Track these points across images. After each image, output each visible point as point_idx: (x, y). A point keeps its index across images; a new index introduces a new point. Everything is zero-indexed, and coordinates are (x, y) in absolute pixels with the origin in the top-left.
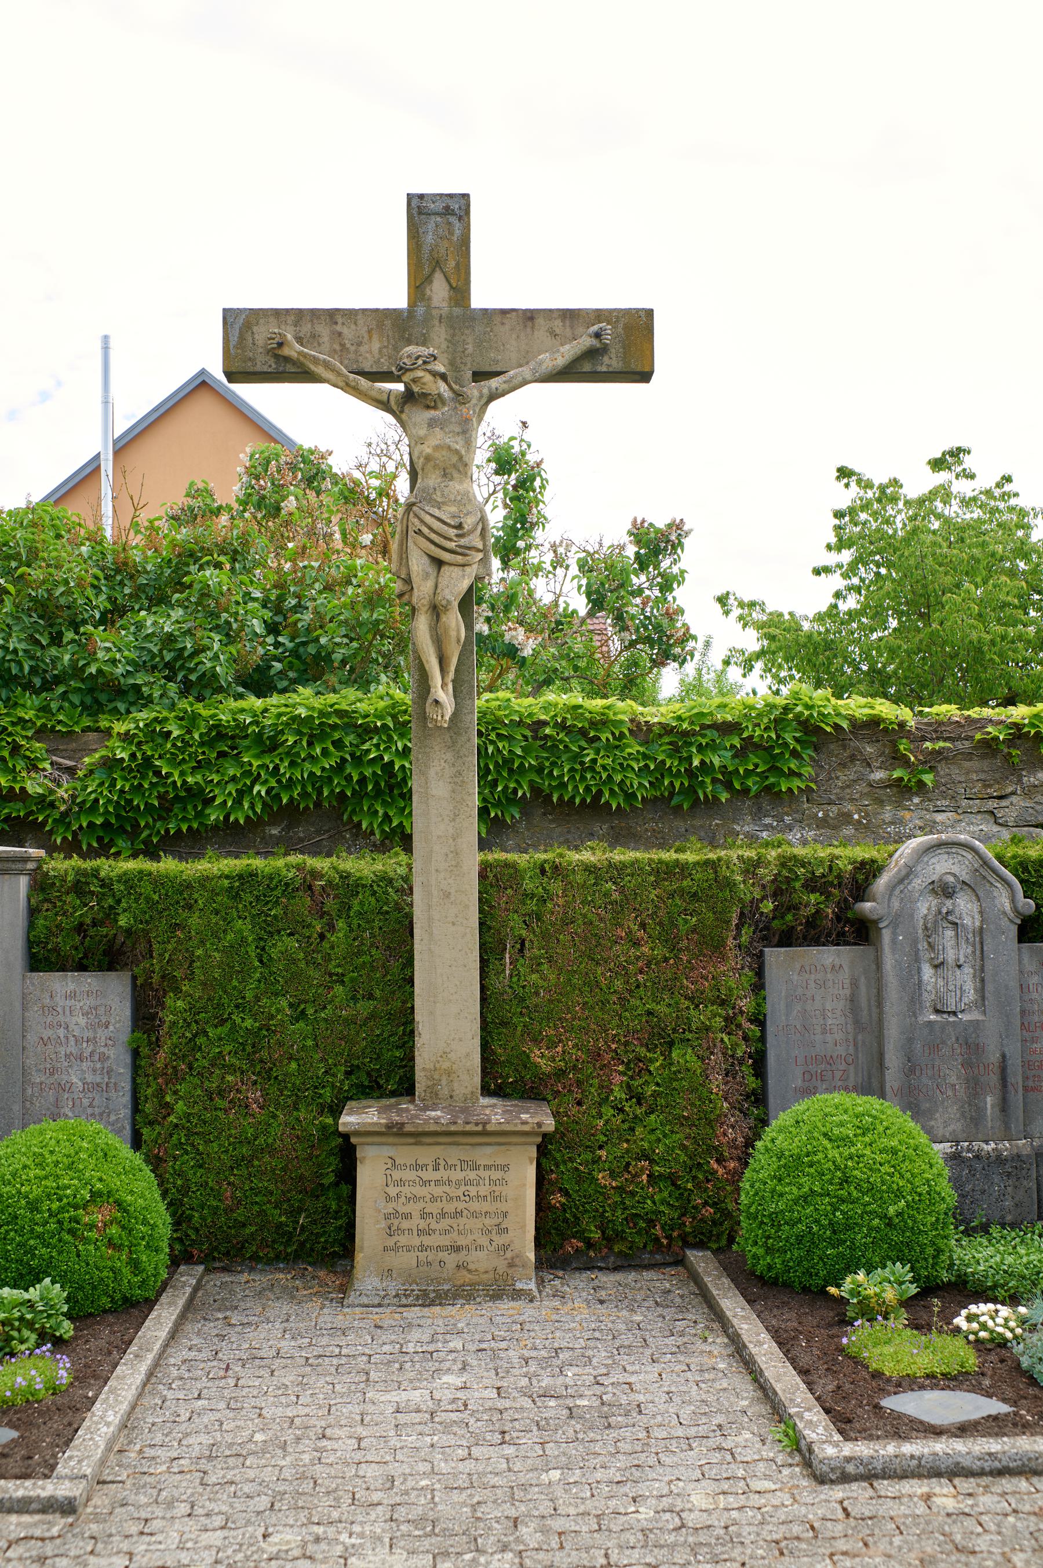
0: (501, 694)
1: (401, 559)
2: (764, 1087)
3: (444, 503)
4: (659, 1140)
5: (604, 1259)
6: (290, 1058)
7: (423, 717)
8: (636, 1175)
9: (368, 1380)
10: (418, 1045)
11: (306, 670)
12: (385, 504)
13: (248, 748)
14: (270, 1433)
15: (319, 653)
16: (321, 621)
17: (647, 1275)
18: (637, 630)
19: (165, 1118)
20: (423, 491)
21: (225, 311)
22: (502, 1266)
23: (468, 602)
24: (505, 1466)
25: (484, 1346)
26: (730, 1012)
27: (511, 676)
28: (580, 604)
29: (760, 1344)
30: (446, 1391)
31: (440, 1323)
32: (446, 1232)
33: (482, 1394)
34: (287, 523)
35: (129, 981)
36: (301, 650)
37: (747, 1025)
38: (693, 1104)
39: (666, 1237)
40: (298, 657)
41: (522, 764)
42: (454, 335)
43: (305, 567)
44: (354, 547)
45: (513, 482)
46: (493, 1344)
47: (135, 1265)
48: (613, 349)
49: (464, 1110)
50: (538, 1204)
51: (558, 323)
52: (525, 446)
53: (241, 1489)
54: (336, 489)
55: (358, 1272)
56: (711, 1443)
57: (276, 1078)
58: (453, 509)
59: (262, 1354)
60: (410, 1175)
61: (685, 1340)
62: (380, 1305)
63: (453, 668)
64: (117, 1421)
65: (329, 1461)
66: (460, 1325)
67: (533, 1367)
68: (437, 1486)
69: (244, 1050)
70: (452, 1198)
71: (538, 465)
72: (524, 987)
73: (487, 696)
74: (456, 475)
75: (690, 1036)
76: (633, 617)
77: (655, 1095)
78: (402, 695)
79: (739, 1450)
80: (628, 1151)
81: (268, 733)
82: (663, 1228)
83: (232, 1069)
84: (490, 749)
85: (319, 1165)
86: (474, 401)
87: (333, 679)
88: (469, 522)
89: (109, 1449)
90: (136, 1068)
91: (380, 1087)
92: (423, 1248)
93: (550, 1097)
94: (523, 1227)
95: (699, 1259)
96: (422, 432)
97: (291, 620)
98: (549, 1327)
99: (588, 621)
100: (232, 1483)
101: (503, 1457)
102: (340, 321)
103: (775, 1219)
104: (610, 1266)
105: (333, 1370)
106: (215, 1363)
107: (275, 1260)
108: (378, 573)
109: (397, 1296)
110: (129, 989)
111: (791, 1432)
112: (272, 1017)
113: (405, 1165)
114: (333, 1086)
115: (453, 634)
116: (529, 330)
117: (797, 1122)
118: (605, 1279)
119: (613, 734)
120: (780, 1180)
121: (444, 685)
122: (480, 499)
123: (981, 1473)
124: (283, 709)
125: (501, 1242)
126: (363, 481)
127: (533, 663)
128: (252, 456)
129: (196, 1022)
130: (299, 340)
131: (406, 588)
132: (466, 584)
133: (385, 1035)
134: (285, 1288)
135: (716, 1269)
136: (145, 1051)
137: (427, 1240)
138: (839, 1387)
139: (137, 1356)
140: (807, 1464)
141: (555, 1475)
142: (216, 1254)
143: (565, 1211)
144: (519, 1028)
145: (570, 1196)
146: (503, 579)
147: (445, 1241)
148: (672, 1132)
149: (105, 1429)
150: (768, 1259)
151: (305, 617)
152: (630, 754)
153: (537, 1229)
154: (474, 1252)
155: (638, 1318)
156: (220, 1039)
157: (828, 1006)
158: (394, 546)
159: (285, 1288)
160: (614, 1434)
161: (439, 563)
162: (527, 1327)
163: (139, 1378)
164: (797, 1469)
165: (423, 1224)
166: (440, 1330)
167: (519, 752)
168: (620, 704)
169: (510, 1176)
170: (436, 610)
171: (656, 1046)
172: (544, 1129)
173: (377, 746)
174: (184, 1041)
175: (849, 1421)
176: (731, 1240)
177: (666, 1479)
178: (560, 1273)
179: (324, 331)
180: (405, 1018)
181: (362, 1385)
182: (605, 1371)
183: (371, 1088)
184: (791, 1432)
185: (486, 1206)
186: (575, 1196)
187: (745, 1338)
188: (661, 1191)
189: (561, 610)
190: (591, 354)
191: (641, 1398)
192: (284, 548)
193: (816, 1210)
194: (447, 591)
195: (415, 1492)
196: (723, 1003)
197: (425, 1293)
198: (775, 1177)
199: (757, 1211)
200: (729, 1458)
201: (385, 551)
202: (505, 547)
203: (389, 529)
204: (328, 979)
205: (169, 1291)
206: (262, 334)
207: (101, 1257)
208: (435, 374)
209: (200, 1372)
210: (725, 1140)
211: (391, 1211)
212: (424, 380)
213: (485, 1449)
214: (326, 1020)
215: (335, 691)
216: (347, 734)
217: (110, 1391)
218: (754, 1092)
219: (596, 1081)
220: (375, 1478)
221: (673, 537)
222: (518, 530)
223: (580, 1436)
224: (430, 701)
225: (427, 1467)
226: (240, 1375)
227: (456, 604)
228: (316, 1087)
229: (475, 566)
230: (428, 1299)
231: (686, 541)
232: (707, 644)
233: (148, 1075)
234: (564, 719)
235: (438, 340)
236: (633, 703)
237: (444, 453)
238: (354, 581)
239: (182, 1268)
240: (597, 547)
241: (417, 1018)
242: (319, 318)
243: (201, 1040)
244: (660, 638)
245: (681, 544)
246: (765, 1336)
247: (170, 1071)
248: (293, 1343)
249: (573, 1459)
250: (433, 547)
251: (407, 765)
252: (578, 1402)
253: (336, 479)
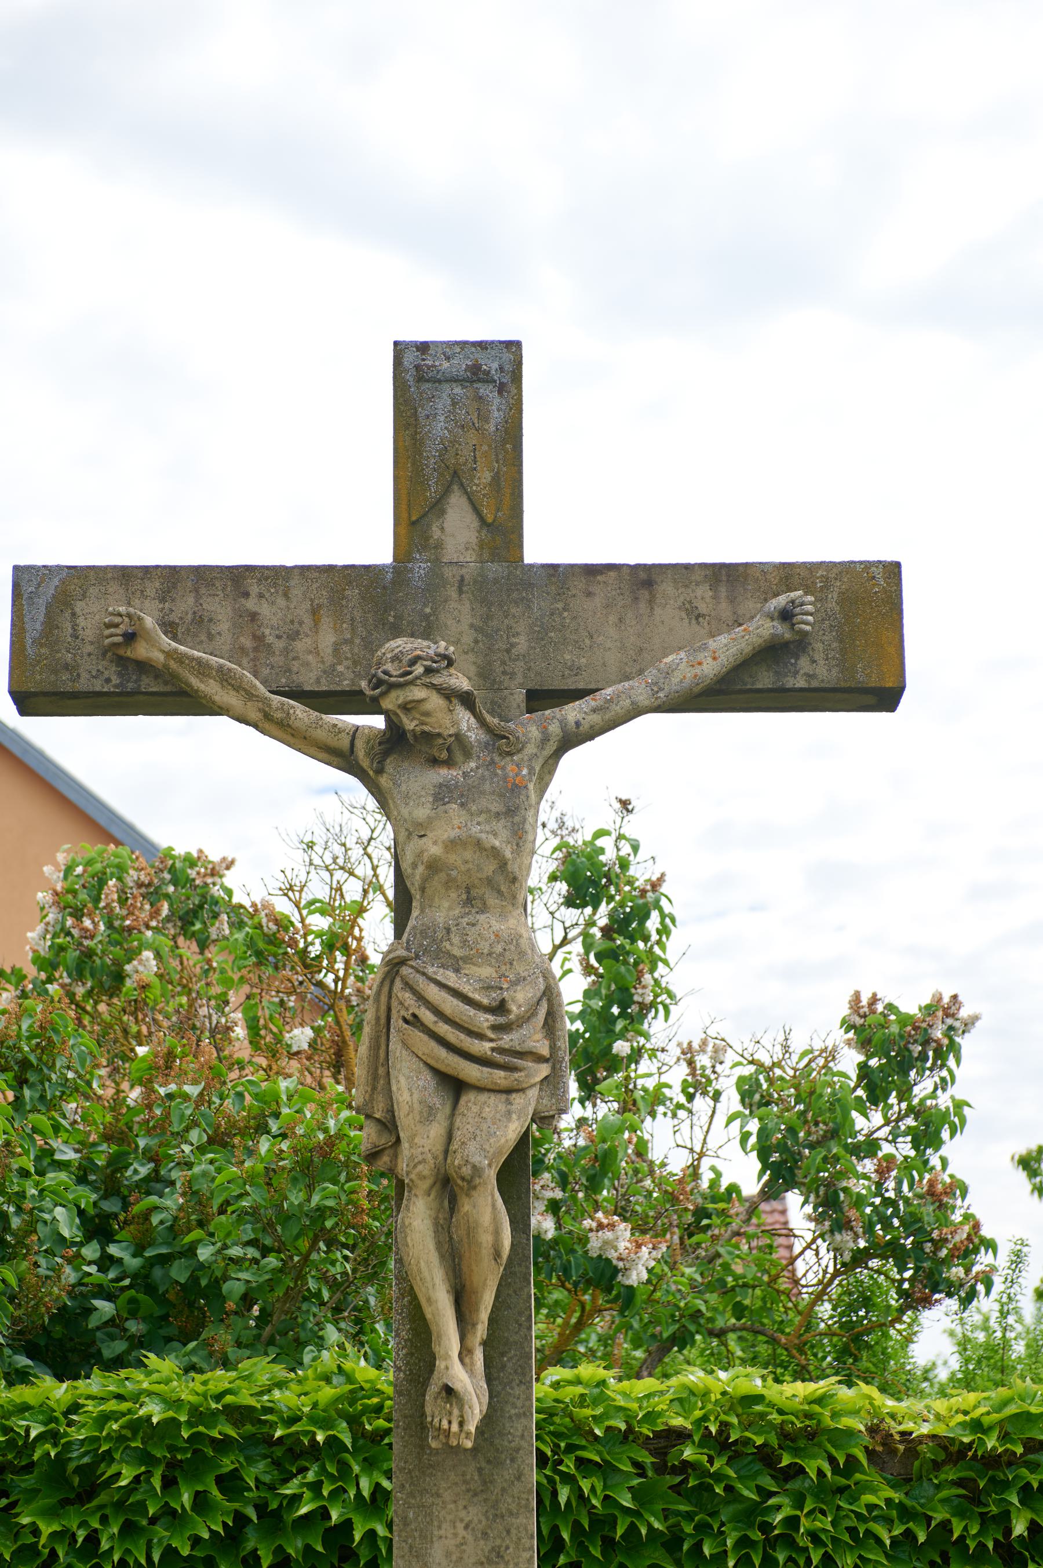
0: (587, 1370)
1: (374, 1077)
3: (466, 959)
7: (419, 1425)
11: (165, 1318)
12: (340, 966)
13: (33, 1494)
15: (194, 1279)
16: (200, 1210)
18: (869, 1229)
20: (424, 934)
21: (19, 571)
23: (517, 1170)
27: (600, 1324)
28: (745, 1173)
34: (136, 1007)
36: (157, 1272)
40: (150, 1289)
41: (633, 1529)
42: (488, 617)
43: (170, 1096)
44: (274, 1055)
45: (603, 922)
48: (819, 642)
51: (704, 592)
52: (626, 849)
54: (239, 936)
58: (486, 972)
63: (484, 1315)
71: (655, 885)
73: (555, 1373)
74: (492, 901)
76: (859, 1201)
78: (372, 1373)
81: (78, 1458)
84: (564, 1494)
86: (530, 749)
87: (223, 1337)
88: (520, 999)
96: (422, 813)
97: (136, 1209)
99: (764, 1207)
102: (254, 590)
108: (324, 1107)
115: (486, 1239)
116: (643, 605)
119: (832, 1460)
121: (465, 1352)
122: (545, 946)
124: (112, 1405)
126: (296, 918)
127: (650, 1300)
128: (69, 870)
130: (170, 628)
131: (385, 1140)
132: (512, 1131)
146: (582, 1122)
151: (168, 1203)
152: (871, 1507)
158: (359, 1055)
161: (455, 1087)
167: (626, 1501)
168: (845, 1393)
170: (450, 1188)
173: (316, 1487)
179: (220, 609)
189: (705, 1184)
190: (773, 653)
192: (128, 1057)
194: (472, 1147)
201: (339, 1064)
202: (587, 1055)
203: (347, 1018)
206: (92, 616)
208: (449, 694)
212: (428, 706)
215: (226, 1364)
216: (250, 1461)
221: (938, 1034)
222: (614, 1020)
224: (433, 1389)
227: (491, 1174)
229: (533, 1093)
231: (965, 1042)
232: (1018, 1259)
234: (724, 1426)
235: (456, 632)
236: (872, 1391)
237: (468, 855)
238: (274, 1126)
240: (778, 1054)
242: (211, 584)
244: (918, 1245)
245: (954, 1048)
250: (443, 1052)
251: (381, 1531)
253: (238, 916)
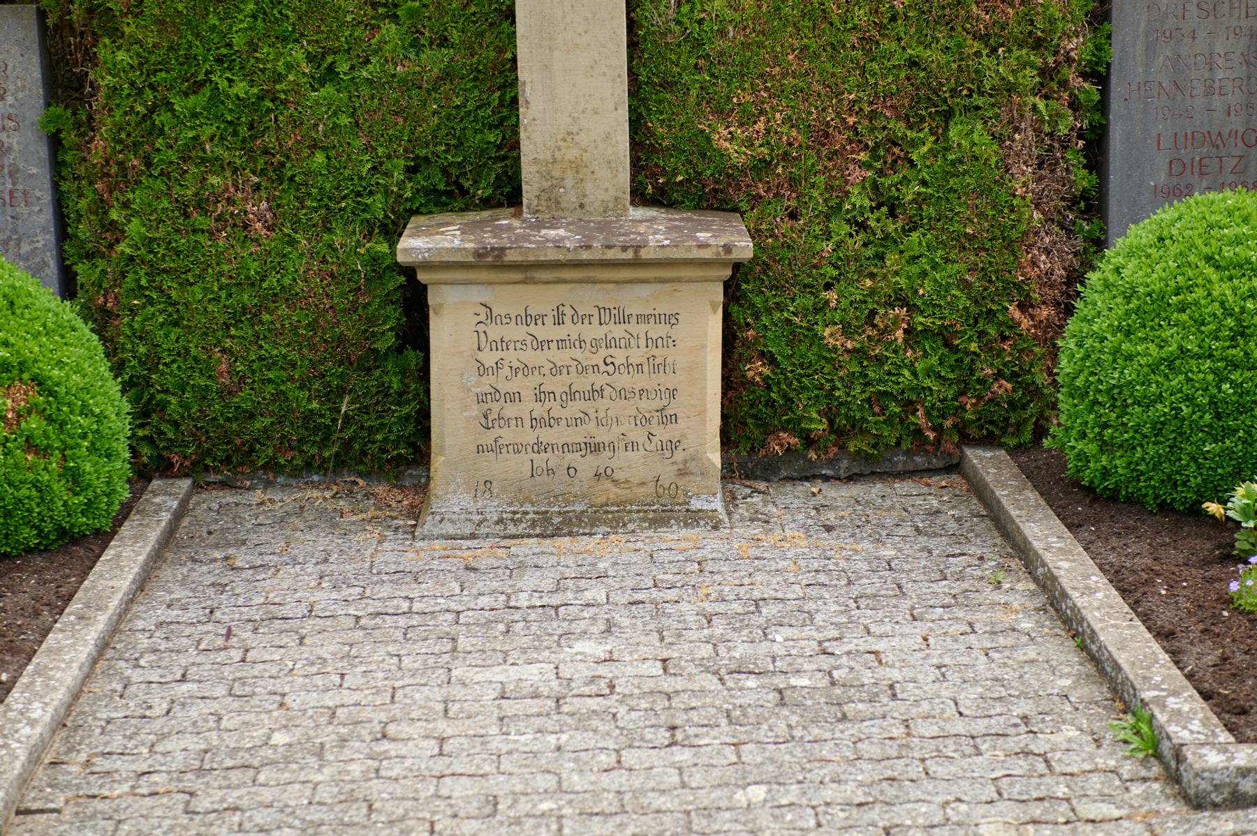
2: (1102, 187)
4: (924, 274)
5: (831, 463)
6: (314, 147)
8: (885, 331)
9: (454, 650)
10: (524, 121)
14: (298, 732)
17: (902, 487)
19: (111, 246)
22: (668, 474)
24: (675, 779)
25: (639, 596)
26: (1051, 60)
29: (1090, 591)
30: (581, 666)
31: (570, 562)
32: (577, 422)
33: (638, 670)
35: (32, 20)
37: (1076, 82)
38: (982, 215)
39: (934, 429)
46: (655, 593)
47: (74, 479)
49: (603, 227)
50: (726, 379)
53: (250, 819)
55: (437, 486)
56: (1012, 744)
57: (292, 179)
59: (284, 611)
60: (517, 332)
61: (966, 585)
62: (473, 536)
64: (47, 718)
65: (393, 774)
66: (601, 565)
67: (719, 628)
68: (567, 811)
69: (235, 133)
70: (585, 369)
72: (700, 22)
75: (978, 101)
77: (920, 200)
79: (1058, 755)
80: (872, 292)
82: (928, 414)
83: (217, 165)
85: (369, 320)
89: (34, 759)
90: (57, 166)
91: (464, 192)
92: (540, 447)
93: (744, 206)
94: (702, 413)
95: (987, 463)
98: (745, 567)
100: (236, 809)
101: (672, 765)
103: (1117, 397)
104: (842, 473)
105: (399, 634)
106: (210, 627)
107: (304, 469)
109: (500, 521)
110: (34, 34)
111: (1145, 728)
112: (279, 78)
113: (508, 316)
114: (387, 193)
117: (1161, 239)
118: (833, 494)
120: (1128, 334)
123: (1094, 659)
125: (666, 438)
129: (152, 87)
133: (471, 106)
134: (322, 512)
135: (1015, 476)
136: (69, 137)
137: (547, 435)
138: (1224, 659)
139: (81, 618)
140: (1173, 778)
141: (758, 793)
142: (209, 462)
143: (769, 388)
144: (694, 92)
145: (778, 365)
147: (576, 435)
148: (947, 260)
149: (27, 731)
150: (1104, 460)
153: (724, 417)
154: (621, 453)
155: (888, 553)
156: (195, 115)
157: (1219, 48)
159: (322, 512)
160: (852, 730)
162: (709, 567)
163: (85, 651)
164: (1156, 786)
165: (539, 411)
166: (569, 573)
169: (678, 332)
171: (922, 119)
172: (736, 255)
174: (132, 119)
175: (1244, 712)
176: (1040, 432)
177: (939, 799)
178: (762, 486)
180: (502, 80)
181: (446, 658)
182: (835, 633)
183: (449, 194)
184: (1145, 728)
185: (640, 381)
186: (784, 364)
187: (1065, 582)
188: (926, 355)
191: (895, 675)
193: (1189, 380)
195: (532, 821)
196: (1038, 44)
197: (545, 517)
198: (1119, 329)
199: (1088, 384)
200: (1041, 767)
204: (370, 12)
205: (135, 518)
207: (16, 465)
209: (185, 641)
210: (1033, 273)
211: (488, 389)
213: (643, 754)
214: (369, 82)
217: (37, 672)
218: (1085, 195)
219: (821, 179)
220: (467, 800)
223: (798, 733)
225: (551, 781)
226: (250, 644)
228: (359, 194)
230: (551, 526)
233: (77, 178)
239: (156, 483)
241: (523, 74)
243: (162, 118)
246: (1097, 579)
247: (114, 169)
248: (334, 595)
249: (786, 768)
252: (794, 681)
